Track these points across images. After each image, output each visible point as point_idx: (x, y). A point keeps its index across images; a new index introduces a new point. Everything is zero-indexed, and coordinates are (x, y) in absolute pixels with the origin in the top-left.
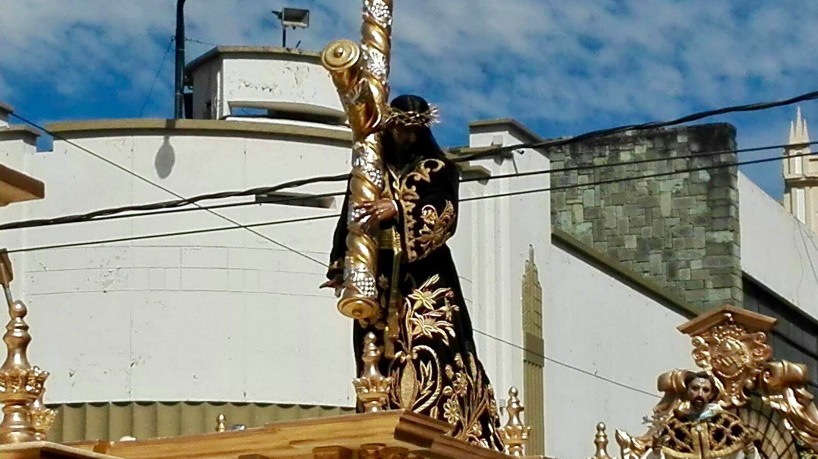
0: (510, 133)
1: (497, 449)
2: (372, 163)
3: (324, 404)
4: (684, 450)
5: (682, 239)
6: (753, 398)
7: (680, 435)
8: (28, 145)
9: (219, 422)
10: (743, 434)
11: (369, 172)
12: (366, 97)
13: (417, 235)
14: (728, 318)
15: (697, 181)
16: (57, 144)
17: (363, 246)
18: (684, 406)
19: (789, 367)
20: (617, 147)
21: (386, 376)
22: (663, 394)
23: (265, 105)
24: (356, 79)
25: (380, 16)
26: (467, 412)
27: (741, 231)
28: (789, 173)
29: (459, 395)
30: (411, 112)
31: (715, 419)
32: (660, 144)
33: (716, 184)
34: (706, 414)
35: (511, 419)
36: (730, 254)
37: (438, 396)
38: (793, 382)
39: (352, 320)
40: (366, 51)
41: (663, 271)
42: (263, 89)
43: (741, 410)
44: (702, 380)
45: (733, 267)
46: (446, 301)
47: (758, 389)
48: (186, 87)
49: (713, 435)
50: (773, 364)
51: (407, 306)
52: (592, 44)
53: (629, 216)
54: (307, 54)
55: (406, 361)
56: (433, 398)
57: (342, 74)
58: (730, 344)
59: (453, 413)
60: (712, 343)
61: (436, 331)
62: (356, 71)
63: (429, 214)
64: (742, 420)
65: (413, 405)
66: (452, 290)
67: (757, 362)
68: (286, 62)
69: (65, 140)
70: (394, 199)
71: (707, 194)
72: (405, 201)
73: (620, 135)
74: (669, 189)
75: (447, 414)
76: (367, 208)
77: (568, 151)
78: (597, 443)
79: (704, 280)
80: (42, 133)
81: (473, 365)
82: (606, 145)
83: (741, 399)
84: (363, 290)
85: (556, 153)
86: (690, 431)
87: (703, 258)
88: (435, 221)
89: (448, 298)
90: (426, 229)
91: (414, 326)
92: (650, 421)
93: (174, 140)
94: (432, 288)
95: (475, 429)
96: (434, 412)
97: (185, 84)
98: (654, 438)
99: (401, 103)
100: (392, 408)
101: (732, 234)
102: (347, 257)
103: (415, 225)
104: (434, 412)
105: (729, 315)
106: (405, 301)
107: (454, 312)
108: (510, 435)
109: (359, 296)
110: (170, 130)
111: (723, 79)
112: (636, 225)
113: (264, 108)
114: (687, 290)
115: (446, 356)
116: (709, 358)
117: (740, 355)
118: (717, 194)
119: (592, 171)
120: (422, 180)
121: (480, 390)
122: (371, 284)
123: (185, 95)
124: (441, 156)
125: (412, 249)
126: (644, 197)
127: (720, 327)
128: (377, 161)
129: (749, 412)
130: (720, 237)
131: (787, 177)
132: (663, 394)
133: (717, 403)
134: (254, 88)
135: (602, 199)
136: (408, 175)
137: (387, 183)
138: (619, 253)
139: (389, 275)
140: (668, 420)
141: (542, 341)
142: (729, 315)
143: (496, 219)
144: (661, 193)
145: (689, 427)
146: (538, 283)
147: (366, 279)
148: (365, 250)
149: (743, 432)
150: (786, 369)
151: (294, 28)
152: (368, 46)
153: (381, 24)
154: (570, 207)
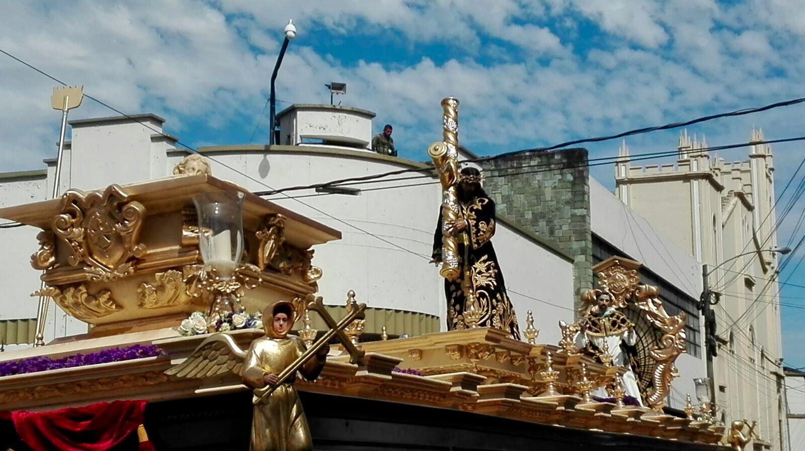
4: (596, 332)
5: (558, 213)
6: (630, 304)
7: (594, 324)
13: (477, 236)
17: (451, 243)
18: (595, 309)
19: (649, 288)
31: (612, 315)
32: (544, 160)
33: (577, 182)
34: (607, 313)
36: (585, 221)
38: (651, 296)
43: (624, 310)
44: (605, 295)
46: (492, 268)
47: (633, 299)
48: (276, 127)
52: (514, 100)
56: (487, 316)
63: (482, 226)
67: (632, 285)
71: (572, 188)
72: (471, 219)
73: (522, 155)
81: (505, 299)
83: (624, 304)
85: (486, 164)
87: (569, 224)
90: (482, 233)
91: (476, 281)
93: (270, 157)
94: (485, 261)
97: (275, 125)
99: (466, 172)
102: (443, 248)
107: (495, 273)
110: (267, 151)
111: (589, 120)
112: (531, 205)
115: (493, 295)
118: (577, 188)
124: (486, 197)
125: (475, 243)
126: (535, 189)
130: (579, 212)
131: (617, 179)
137: (460, 211)
144: (545, 187)
145: (599, 320)
148: (452, 245)
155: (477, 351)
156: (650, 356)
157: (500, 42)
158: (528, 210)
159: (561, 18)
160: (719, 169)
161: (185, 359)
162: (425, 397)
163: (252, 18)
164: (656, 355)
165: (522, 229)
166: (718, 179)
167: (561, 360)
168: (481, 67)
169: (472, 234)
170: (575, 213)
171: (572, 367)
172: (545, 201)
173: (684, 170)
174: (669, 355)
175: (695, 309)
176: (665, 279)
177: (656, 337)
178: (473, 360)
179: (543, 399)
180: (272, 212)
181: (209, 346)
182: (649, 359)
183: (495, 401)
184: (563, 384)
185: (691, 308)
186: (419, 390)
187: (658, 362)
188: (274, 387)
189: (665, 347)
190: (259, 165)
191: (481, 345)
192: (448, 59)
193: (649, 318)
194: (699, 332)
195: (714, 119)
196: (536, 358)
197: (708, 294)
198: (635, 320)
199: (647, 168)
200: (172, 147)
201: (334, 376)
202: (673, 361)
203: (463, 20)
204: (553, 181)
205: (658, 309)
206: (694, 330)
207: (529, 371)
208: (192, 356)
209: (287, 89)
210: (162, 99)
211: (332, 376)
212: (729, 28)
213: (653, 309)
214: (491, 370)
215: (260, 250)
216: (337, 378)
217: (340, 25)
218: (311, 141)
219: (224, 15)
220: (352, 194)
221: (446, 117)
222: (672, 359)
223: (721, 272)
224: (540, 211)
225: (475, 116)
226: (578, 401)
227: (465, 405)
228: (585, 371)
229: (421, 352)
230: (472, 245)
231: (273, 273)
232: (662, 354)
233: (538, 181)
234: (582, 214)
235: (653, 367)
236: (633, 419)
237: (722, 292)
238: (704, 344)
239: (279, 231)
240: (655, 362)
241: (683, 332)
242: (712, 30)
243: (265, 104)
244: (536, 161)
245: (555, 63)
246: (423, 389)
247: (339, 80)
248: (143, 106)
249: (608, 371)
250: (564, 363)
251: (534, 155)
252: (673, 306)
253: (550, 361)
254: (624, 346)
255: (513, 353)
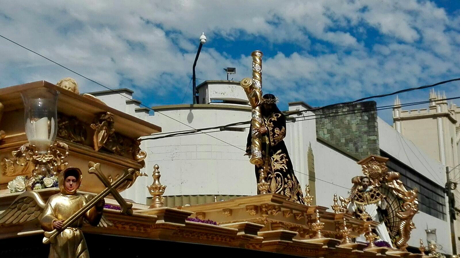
0: (302, 106)
1: (302, 204)
2: (258, 116)
3: (244, 195)
4: (362, 202)
5: (360, 139)
6: (383, 184)
7: (360, 197)
8: (146, 114)
9: (215, 199)
10: (380, 196)
11: (257, 118)
12: (255, 95)
13: (273, 137)
14: (373, 159)
15: (364, 120)
16: (155, 113)
18: (360, 188)
19: (394, 173)
20: (337, 110)
21: (268, 183)
22: (354, 184)
23: (222, 99)
24: (252, 90)
25: (258, 70)
26: (292, 193)
27: (379, 136)
28: (395, 116)
29: (289, 187)
30: (270, 99)
31: (371, 191)
32: (351, 108)
33: (370, 121)
34: (368, 190)
35: (307, 194)
36: (376, 143)
37: (283, 188)
39: (254, 165)
40: (254, 81)
41: (354, 149)
42: (221, 94)
43: (379, 188)
45: (376, 148)
47: (385, 181)
48: (197, 94)
49: (371, 196)
50: (388, 173)
51: (272, 160)
52: (332, 75)
53: (342, 132)
54: (235, 82)
55: (272, 177)
56: (281, 189)
57: (248, 88)
58: (374, 167)
59: (288, 193)
60: (368, 167)
61: (281, 167)
62: (252, 87)
63: (277, 131)
64: (380, 191)
65: (275, 191)
66: (285, 154)
68: (229, 85)
69: (158, 112)
70: (266, 127)
72: (269, 127)
73: (338, 106)
74: (355, 123)
75: (286, 193)
76: (257, 130)
77: (321, 111)
78: (334, 200)
79: (367, 152)
80: (151, 110)
81: (293, 177)
82: (333, 109)
83: (379, 184)
84: (258, 156)
86: (363, 195)
88: (279, 133)
89: (284, 157)
90: (276, 135)
91: (274, 166)
92: (350, 193)
93: (193, 111)
94: (279, 154)
95: (295, 198)
96: (282, 193)
97: (196, 93)
98: (351, 198)
99: (266, 97)
100: (269, 192)
101: (376, 137)
102: (252, 146)
103: (273, 134)
104: (282, 193)
105: (373, 158)
106: (271, 158)
107: (286, 161)
108: (307, 199)
109: (257, 158)
110: (191, 108)
111: (375, 85)
113: (222, 100)
114: (362, 155)
115: (285, 175)
116: (368, 172)
117: (378, 170)
118: (371, 124)
119: (329, 118)
120: (274, 120)
121: (296, 185)
122: (260, 153)
123: (196, 96)
125: (272, 142)
127: (371, 162)
128: (259, 115)
129: (382, 188)
130: (372, 138)
132: (354, 184)
133: (371, 186)
134: (218, 94)
135: (333, 126)
136: (270, 119)
137: (263, 122)
138: (339, 143)
139: (265, 151)
140: (356, 192)
141: (315, 173)
142: (373, 158)
143: (298, 134)
144: (352, 124)
145: (363, 194)
146: (313, 154)
147: (258, 152)
148: (257, 143)
149: (380, 195)
150: (393, 174)
151: (231, 74)
152: (255, 79)
153: (258, 72)
154: (322, 129)
155: (266, 209)
156: (397, 216)
157: (322, 42)
158: (343, 138)
159: (356, 27)
160: (454, 111)
161: (4, 211)
162: (218, 239)
163: (181, 33)
164: (400, 215)
165: (338, 148)
166: (453, 117)
167: (331, 216)
168: (311, 56)
169: (270, 136)
170: (370, 138)
171: (339, 221)
172: (352, 132)
173: (433, 112)
174: (408, 215)
175: (442, 192)
176: (423, 175)
177: (400, 204)
178: (264, 215)
179: (370, 250)
180: (103, 111)
181: (21, 200)
182: (396, 218)
183: (274, 242)
184: (333, 232)
185: (440, 192)
186: (212, 234)
187: (402, 219)
188: (60, 230)
189: (406, 210)
190: (187, 115)
191: (270, 205)
192: (292, 53)
193: (394, 192)
194: (445, 206)
195: (449, 82)
196: (312, 214)
197: (450, 184)
198: (386, 194)
199: (411, 111)
200: (138, 107)
201: (139, 224)
202: (411, 219)
203: (300, 30)
204: (357, 120)
205: (400, 186)
206: (442, 205)
207: (308, 223)
208: (10, 208)
209: (201, 72)
210: (131, 80)
211: (136, 224)
212: (455, 30)
213: (397, 186)
214: (280, 223)
215: (95, 137)
216: (143, 225)
217: (230, 35)
218: (218, 101)
219: (165, 32)
220: (241, 131)
221: (254, 63)
222: (410, 217)
223: (457, 171)
224: (349, 138)
225: (309, 84)
226: (387, 250)
227: (254, 244)
228: (346, 223)
229: (231, 211)
230: (271, 143)
231: (108, 154)
232: (403, 214)
233: (348, 120)
234: (374, 139)
235: (399, 223)
236: (380, 254)
237: (458, 183)
238: (449, 213)
239: (109, 124)
240: (400, 220)
241: (416, 200)
242: (445, 31)
243: (189, 81)
244: (347, 109)
245: (354, 53)
246: (216, 233)
247: (231, 66)
248: (120, 85)
249: (365, 224)
250: (333, 219)
251: (345, 106)
252: (429, 192)
253: (318, 216)
254: (379, 210)
255: (294, 212)
